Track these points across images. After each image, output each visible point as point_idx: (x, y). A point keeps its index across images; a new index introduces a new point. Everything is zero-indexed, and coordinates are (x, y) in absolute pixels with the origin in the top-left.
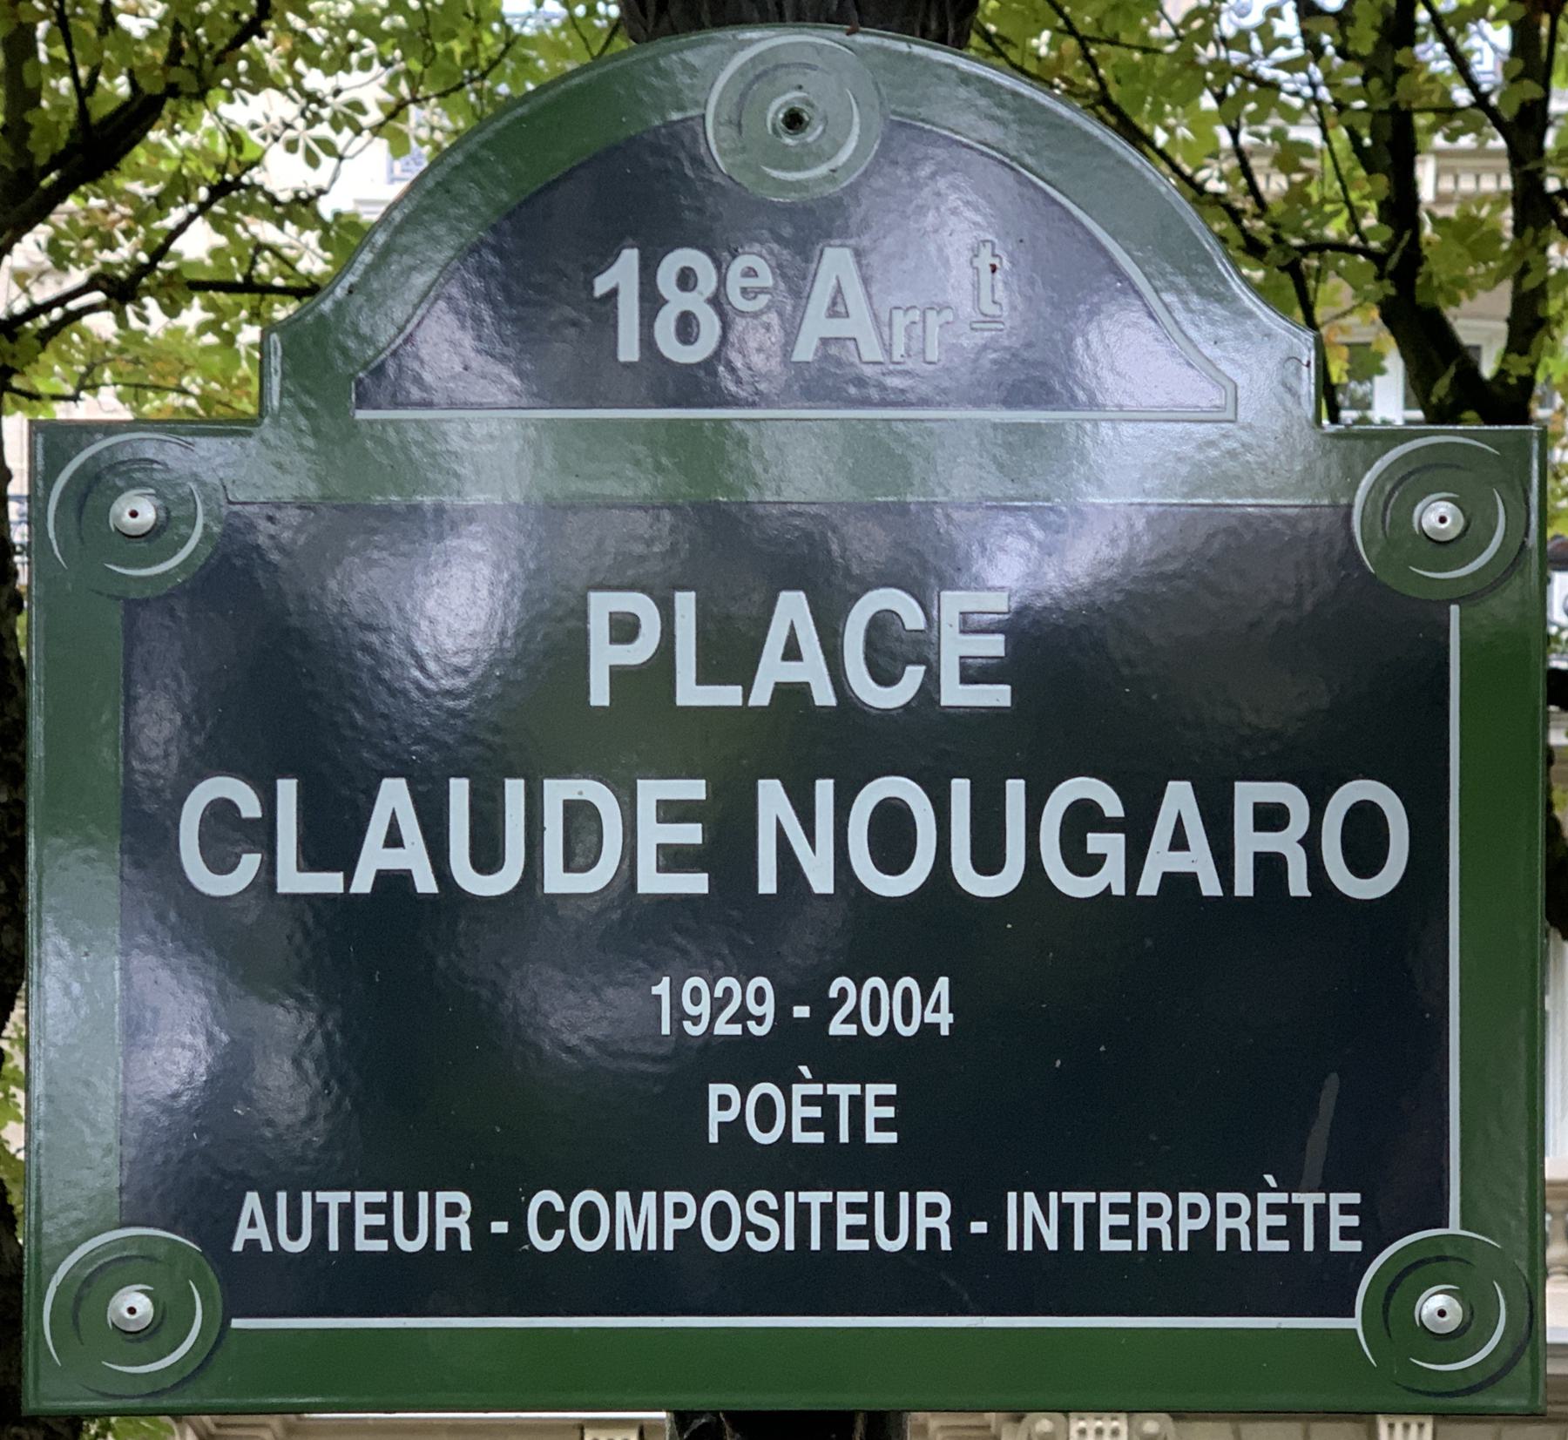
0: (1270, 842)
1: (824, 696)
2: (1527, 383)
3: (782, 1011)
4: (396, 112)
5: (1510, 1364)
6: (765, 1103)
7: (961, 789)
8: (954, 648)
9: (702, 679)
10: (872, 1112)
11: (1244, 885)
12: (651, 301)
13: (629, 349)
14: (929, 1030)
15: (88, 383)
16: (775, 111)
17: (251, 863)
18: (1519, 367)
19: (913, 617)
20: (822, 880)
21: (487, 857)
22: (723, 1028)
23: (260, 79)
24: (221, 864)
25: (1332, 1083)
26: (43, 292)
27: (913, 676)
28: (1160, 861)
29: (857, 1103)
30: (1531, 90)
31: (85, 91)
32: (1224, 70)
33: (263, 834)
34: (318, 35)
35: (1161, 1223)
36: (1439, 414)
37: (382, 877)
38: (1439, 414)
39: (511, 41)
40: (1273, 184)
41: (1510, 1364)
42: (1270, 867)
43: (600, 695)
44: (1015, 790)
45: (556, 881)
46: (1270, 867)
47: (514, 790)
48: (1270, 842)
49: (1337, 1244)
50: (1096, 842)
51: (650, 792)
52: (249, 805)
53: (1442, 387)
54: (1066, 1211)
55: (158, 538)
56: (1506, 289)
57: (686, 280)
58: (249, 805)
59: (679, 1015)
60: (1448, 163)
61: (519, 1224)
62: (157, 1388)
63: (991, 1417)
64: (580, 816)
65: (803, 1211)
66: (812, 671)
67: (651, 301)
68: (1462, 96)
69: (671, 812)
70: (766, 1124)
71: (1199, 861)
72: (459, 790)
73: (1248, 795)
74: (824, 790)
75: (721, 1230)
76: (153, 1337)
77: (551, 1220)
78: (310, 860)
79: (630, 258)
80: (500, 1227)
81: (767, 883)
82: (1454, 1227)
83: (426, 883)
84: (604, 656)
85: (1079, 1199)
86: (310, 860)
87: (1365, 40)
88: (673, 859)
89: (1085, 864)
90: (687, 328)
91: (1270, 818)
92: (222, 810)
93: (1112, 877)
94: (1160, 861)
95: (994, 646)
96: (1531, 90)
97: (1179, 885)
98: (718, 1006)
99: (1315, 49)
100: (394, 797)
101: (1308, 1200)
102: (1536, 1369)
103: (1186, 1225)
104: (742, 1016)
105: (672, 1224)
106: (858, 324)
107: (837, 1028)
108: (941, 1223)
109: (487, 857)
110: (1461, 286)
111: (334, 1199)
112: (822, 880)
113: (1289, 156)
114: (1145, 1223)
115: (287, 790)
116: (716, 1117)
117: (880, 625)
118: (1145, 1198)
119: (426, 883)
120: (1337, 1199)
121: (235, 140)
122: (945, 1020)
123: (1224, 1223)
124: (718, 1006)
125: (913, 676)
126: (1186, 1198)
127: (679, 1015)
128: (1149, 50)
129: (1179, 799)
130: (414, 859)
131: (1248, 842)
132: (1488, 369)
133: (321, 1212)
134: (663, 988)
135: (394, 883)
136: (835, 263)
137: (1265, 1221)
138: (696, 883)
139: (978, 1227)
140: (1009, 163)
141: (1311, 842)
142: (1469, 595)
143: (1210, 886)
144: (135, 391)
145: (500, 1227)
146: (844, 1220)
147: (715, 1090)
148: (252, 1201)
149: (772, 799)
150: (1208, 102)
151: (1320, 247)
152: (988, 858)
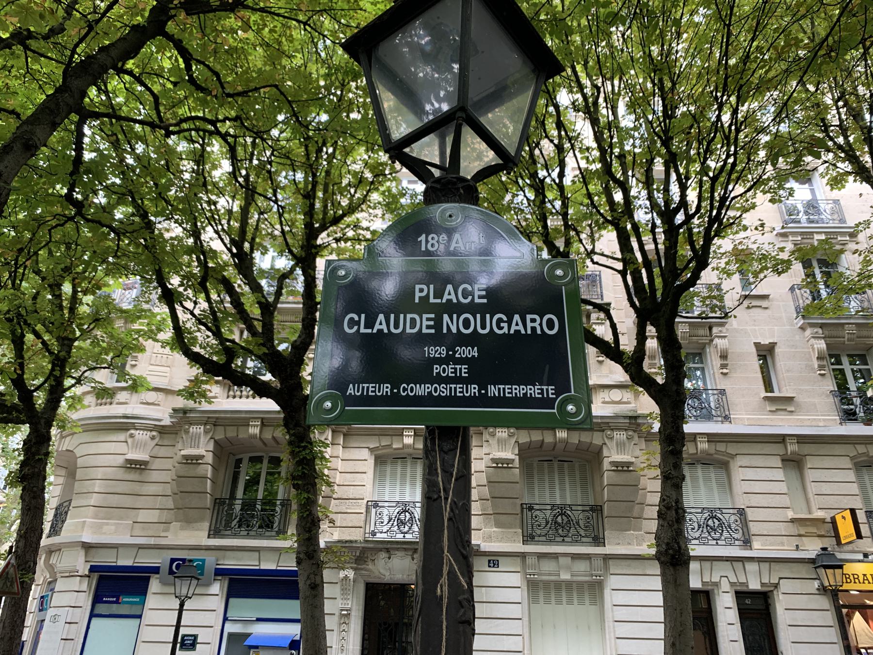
0: (533, 325)
1: (455, 301)
2: (569, 252)
3: (447, 353)
4: (384, 215)
5: (585, 420)
6: (444, 369)
7: (478, 316)
8: (477, 293)
9: (434, 298)
10: (463, 370)
11: (529, 332)
12: (427, 242)
13: (423, 249)
14: (473, 356)
15: (331, 253)
16: (448, 214)
17: (356, 328)
18: (567, 250)
19: (470, 288)
20: (454, 330)
21: (396, 326)
22: (437, 356)
23: (362, 211)
24: (351, 328)
25: (547, 367)
26: (325, 241)
27: (470, 298)
28: (514, 328)
29: (461, 369)
30: (565, 210)
31: (335, 213)
32: (515, 208)
33: (358, 323)
34: (372, 205)
35: (517, 391)
36: (553, 257)
37: (378, 330)
38: (553, 257)
39: (402, 206)
40: (524, 224)
41: (585, 420)
42: (534, 329)
43: (417, 301)
44: (488, 316)
45: (408, 330)
46: (534, 329)
47: (402, 316)
48: (533, 325)
49: (551, 396)
50: (502, 325)
51: (425, 316)
52: (356, 318)
53: (554, 253)
54: (499, 389)
55: (345, 277)
56: (563, 239)
57: (433, 238)
58: (356, 318)
59: (429, 353)
60: (552, 220)
61: (399, 390)
62: (331, 420)
63: (481, 428)
64: (413, 321)
65: (451, 388)
66: (453, 297)
67: (427, 242)
68: (554, 211)
69: (428, 319)
70: (444, 372)
71: (521, 327)
72: (392, 316)
73: (529, 317)
74: (455, 316)
75: (436, 392)
76: (331, 410)
77: (405, 390)
78: (366, 327)
79: (424, 236)
80: (483, 392)
81: (445, 331)
82: (573, 393)
83: (386, 331)
84: (418, 295)
85: (501, 387)
86: (366, 327)
87: (538, 203)
88: (428, 327)
89: (501, 328)
90: (432, 245)
91: (533, 321)
92: (352, 319)
93: (505, 330)
94: (514, 328)
95: (484, 293)
96: (565, 210)
97: (517, 332)
98: (436, 352)
99: (529, 205)
100: (381, 317)
101: (545, 388)
102: (591, 421)
103: (522, 392)
104: (440, 353)
105: (427, 390)
106: (461, 245)
107: (457, 356)
108: (476, 391)
109: (396, 326)
110: (555, 238)
111: (366, 385)
112: (454, 330)
113: (526, 220)
114: (514, 391)
115: (363, 316)
116: (435, 371)
117: (464, 290)
118: (514, 387)
119: (386, 331)
120: (550, 387)
121: (358, 219)
122: (476, 354)
123: (529, 392)
124: (436, 352)
125: (470, 298)
126: (522, 387)
127: (429, 353)
128: (503, 205)
129: (517, 317)
130: (384, 327)
131: (529, 325)
132: (561, 250)
133: (363, 388)
134: (426, 349)
135: (380, 331)
136: (457, 236)
137: (537, 391)
138: (433, 331)
139: (395, 391)
140: (481, 220)
141: (541, 325)
142: (565, 285)
143: (523, 332)
144: (338, 255)
145: (395, 391)
146: (458, 390)
147: (435, 366)
148: (351, 386)
149: (446, 317)
150: (512, 212)
151: (532, 232)
152: (483, 327)
